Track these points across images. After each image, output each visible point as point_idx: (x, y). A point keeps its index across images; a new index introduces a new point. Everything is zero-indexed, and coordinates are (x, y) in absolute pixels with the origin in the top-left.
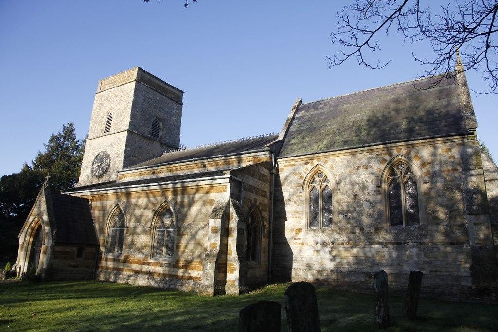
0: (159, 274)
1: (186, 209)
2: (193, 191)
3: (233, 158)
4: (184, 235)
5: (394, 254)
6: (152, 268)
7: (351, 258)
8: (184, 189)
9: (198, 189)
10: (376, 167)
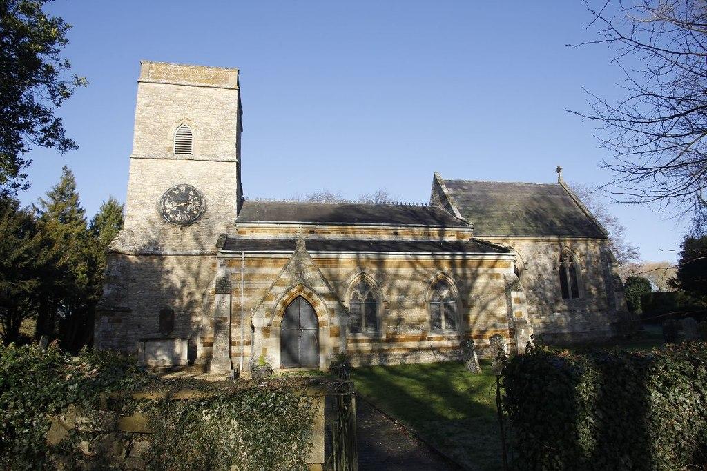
0: (448, 348)
1: (469, 281)
2: (476, 264)
3: (435, 231)
4: (472, 307)
5: (569, 319)
6: (435, 343)
7: (541, 324)
8: (464, 263)
9: (480, 264)
10: (552, 253)
